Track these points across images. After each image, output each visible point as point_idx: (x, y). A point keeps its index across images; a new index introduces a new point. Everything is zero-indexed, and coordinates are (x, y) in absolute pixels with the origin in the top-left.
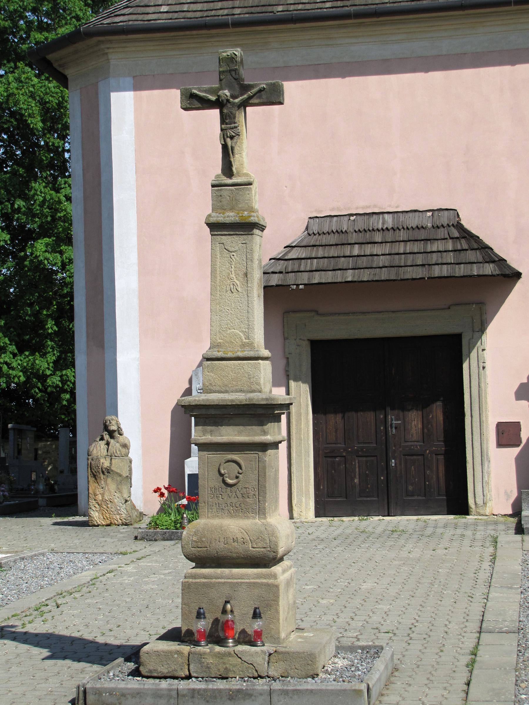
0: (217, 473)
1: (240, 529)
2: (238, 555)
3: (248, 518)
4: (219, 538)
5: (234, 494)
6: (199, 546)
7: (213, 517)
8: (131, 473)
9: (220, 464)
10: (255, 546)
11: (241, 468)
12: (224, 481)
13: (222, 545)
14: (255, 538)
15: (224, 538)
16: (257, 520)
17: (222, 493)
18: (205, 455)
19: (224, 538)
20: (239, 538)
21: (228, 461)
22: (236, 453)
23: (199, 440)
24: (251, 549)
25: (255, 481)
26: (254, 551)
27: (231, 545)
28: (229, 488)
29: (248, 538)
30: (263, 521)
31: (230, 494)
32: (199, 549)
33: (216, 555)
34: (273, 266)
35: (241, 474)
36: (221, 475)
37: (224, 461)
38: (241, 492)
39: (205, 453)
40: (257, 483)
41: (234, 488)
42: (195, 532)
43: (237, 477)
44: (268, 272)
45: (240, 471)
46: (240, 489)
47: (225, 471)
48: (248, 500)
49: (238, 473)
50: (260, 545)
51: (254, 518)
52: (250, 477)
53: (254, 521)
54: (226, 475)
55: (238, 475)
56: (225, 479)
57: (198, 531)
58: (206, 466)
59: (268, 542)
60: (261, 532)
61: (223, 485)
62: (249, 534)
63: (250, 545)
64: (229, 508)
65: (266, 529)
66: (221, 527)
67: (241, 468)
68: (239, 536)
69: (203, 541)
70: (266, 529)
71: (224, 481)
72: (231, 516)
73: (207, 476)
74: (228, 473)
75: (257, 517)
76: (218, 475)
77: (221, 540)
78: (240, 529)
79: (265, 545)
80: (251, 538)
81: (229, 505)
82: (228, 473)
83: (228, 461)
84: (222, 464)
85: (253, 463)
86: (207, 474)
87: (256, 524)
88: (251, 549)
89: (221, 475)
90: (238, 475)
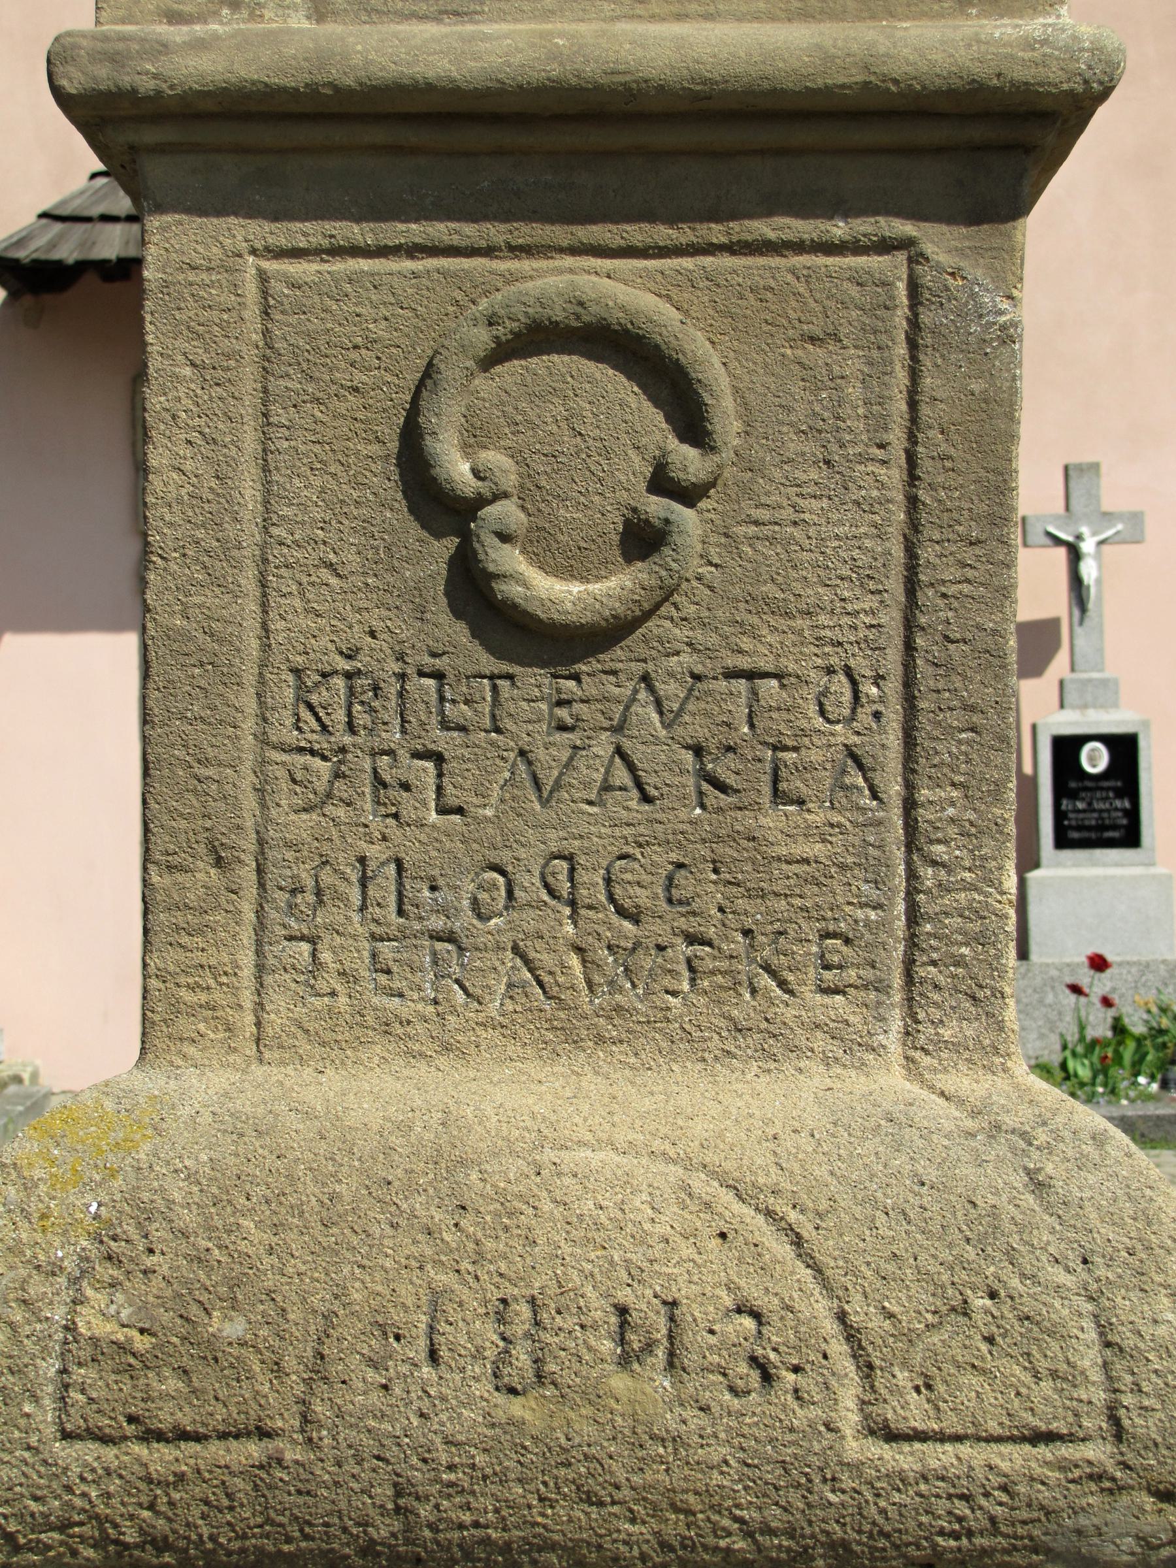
0: (384, 482)
1: (699, 1183)
2: (674, 1527)
3: (772, 1044)
4: (436, 1301)
5: (603, 746)
6: (166, 1417)
7: (331, 1040)
8: (70, 1092)
9: (429, 371)
10: (914, 1412)
11: (691, 422)
12: (472, 591)
13: (468, 1403)
14: (911, 1302)
15: (502, 1311)
16: (890, 1081)
17: (441, 740)
18: (229, 266)
19: (502, 1311)
20: (693, 1311)
21: (537, 337)
22: (637, 233)
23: (164, 48)
24: (856, 1447)
25: (866, 580)
26: (901, 1480)
27: (594, 1396)
28: (535, 680)
29: (820, 1309)
30: (961, 1081)
31: (551, 753)
32: (161, 1458)
33: (383, 1529)
34: (105, 197)
35: (689, 495)
36: (434, 502)
37: (482, 338)
38: (695, 728)
39: (241, 231)
40: (892, 619)
41: (600, 682)
42: (105, 1234)
43: (642, 540)
44: (86, 213)
45: (689, 462)
46: (670, 690)
47: (493, 458)
48: (772, 821)
49: (662, 482)
50: (975, 1398)
51: (858, 1047)
52: (798, 541)
53: (855, 1082)
54: (506, 512)
55: (656, 507)
56: (509, 560)
57: (145, 1216)
58: (248, 407)
59: (1089, 1358)
60: (985, 1230)
61: (460, 632)
62: (824, 1247)
63: (849, 1395)
64: (529, 920)
65: (1038, 1184)
66: (449, 1161)
67: (691, 422)
68: (701, 1280)
69: (213, 1353)
70: (1038, 1184)
71: (472, 591)
72: (560, 1023)
73: (251, 535)
74: (529, 493)
75: (892, 1040)
76: (396, 514)
77: (453, 1336)
78: (699, 1183)
79: (1045, 1405)
80: (857, 1310)
81: (529, 884)
82: (529, 493)
83: (537, 337)
84: (451, 371)
85: (852, 363)
86: (249, 492)
87: (895, 1123)
88: (856, 1447)
89: (434, 502)
90: (656, 507)
